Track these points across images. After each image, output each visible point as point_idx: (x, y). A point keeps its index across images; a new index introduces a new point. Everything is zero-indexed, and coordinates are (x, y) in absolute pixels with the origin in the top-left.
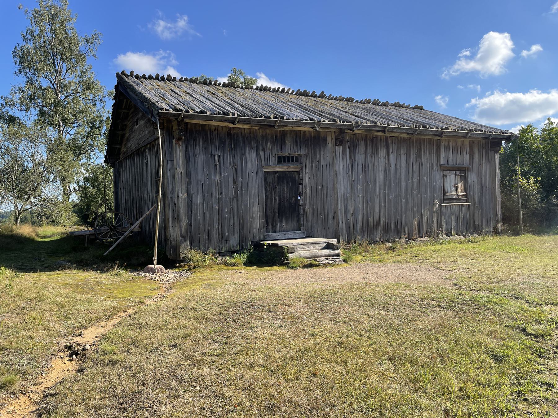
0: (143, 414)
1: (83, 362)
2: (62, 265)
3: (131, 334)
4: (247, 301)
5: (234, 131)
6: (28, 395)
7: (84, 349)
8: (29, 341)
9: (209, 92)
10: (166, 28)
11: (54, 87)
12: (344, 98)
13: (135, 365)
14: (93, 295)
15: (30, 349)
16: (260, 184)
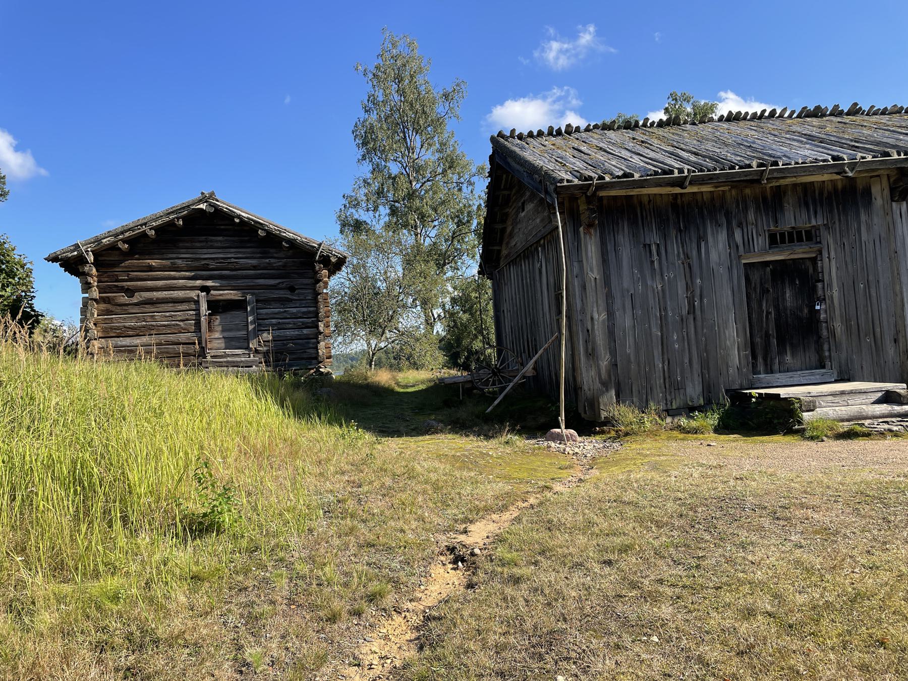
0: (569, 668)
1: (474, 573)
2: (432, 427)
3: (537, 537)
4: (729, 496)
5: (684, 199)
6: (403, 616)
7: (473, 554)
8: (400, 535)
9: (635, 141)
10: (561, 51)
11: (406, 172)
12: (902, 108)
13: (548, 587)
14: (478, 473)
15: (402, 548)
16: (736, 288)
